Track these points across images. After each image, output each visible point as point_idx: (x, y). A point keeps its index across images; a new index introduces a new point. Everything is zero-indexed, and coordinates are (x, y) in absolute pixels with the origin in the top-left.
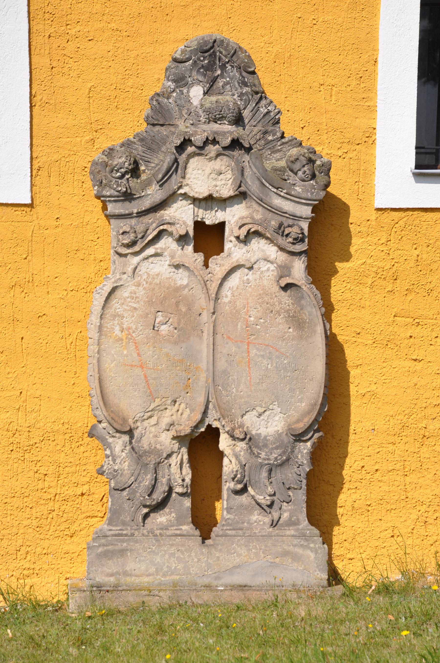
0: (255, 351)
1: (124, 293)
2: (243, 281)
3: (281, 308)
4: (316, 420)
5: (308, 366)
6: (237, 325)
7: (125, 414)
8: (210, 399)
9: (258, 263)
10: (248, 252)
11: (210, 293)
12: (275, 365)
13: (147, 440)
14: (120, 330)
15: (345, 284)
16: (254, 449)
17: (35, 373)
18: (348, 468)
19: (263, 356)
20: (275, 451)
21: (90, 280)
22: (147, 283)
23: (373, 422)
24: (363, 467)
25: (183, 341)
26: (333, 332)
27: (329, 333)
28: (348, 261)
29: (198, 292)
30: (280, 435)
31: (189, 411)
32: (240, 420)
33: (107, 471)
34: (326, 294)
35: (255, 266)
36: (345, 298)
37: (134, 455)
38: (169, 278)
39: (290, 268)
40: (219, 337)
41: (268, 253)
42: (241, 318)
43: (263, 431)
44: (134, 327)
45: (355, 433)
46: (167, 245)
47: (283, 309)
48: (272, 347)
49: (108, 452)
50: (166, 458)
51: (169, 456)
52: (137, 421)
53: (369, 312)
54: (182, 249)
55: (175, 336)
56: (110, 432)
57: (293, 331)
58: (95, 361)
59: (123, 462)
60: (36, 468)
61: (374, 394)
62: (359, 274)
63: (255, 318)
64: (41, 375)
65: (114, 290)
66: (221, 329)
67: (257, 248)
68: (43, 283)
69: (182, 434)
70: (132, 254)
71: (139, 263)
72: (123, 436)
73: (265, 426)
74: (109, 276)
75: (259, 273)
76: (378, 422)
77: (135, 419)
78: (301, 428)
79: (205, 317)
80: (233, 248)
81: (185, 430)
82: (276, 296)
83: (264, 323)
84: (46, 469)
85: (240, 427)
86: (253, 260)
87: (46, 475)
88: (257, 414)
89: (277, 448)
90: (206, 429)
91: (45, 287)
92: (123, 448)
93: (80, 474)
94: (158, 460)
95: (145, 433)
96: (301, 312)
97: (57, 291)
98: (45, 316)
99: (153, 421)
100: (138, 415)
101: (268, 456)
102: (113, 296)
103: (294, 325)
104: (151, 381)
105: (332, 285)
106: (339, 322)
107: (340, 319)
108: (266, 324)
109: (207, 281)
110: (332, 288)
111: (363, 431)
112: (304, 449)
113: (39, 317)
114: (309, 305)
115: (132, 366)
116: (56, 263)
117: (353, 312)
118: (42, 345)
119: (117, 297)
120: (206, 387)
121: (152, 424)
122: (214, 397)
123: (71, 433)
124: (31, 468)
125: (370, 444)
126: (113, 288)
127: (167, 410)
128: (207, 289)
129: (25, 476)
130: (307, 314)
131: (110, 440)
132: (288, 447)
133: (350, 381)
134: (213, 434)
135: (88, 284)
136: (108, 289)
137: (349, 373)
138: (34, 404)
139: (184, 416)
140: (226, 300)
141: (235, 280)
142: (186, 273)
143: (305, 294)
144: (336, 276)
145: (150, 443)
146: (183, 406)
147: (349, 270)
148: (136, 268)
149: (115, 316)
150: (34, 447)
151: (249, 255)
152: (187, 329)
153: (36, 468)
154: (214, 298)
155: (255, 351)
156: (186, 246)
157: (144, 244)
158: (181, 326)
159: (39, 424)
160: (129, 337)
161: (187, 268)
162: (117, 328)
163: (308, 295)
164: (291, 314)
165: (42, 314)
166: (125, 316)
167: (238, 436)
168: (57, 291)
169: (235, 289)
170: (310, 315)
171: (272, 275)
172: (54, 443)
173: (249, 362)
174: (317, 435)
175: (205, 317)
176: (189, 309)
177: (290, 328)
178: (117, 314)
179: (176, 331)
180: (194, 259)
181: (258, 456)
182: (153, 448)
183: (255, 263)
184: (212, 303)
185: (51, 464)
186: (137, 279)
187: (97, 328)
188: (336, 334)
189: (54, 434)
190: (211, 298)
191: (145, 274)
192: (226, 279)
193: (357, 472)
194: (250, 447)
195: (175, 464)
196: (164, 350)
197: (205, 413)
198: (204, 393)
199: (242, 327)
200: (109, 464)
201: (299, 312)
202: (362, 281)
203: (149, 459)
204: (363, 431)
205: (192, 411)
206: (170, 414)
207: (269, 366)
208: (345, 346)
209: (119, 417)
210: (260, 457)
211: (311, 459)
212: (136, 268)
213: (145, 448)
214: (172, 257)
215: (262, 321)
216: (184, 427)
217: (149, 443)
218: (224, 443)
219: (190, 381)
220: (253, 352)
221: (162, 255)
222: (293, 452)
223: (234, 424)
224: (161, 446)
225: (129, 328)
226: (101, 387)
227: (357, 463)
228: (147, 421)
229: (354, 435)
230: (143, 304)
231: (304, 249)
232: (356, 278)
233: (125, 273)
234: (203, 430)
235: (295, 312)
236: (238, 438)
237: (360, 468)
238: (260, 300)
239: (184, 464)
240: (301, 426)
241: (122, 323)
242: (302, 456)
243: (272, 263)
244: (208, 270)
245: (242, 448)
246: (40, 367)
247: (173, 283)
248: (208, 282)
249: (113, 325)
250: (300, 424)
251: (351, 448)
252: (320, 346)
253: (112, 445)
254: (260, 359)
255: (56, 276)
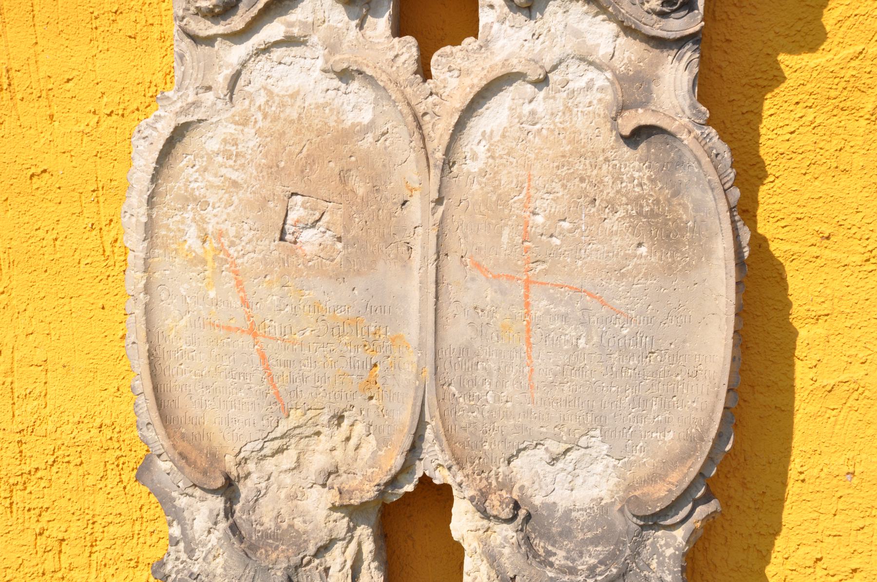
0: (545, 302)
1: (205, 142)
2: (520, 117)
3: (618, 192)
4: (701, 474)
5: (684, 342)
6: (500, 234)
7: (215, 444)
8: (427, 418)
9: (562, 67)
10: (536, 36)
11: (430, 146)
12: (596, 339)
13: (270, 507)
14: (199, 237)
15: (799, 111)
16: (537, 541)
17: (30, 308)
18: (780, 560)
19: (564, 317)
20: (590, 548)
21: (153, 89)
22: (265, 117)
23: (850, 455)
24: (819, 559)
25: (358, 273)
26: (760, 231)
27: (746, 254)
28: (813, 49)
29: (401, 142)
30: (605, 510)
31: (374, 443)
32: (503, 469)
33: (173, 576)
34: (748, 137)
35: (553, 77)
36: (796, 146)
37: (237, 545)
38: (325, 106)
39: (649, 82)
40: (451, 263)
41: (591, 40)
42: (510, 216)
43: (562, 499)
44: (232, 231)
45: (803, 481)
46: (320, 15)
47: (625, 195)
48: (590, 295)
49: (176, 531)
50: (315, 556)
51: (323, 550)
52: (246, 460)
53: (861, 183)
54: (361, 26)
55: (338, 259)
56: (180, 484)
57: (650, 251)
58: (139, 311)
59: (210, 557)
60: (40, 525)
61: (857, 389)
62: (843, 84)
63: (548, 218)
64: (47, 313)
65: (179, 133)
66: (455, 243)
67: (561, 27)
68: (36, 94)
69: (356, 501)
70: (226, 36)
71: (246, 61)
72: (209, 496)
73: (567, 485)
74: (169, 94)
75: (565, 95)
76: (864, 456)
77: (242, 455)
78: (659, 499)
79: (416, 210)
80: (496, 26)
81: (362, 491)
82: (607, 160)
83: (571, 231)
84: (63, 529)
85: (501, 486)
86: (548, 61)
87: (63, 540)
88: (547, 457)
89: (595, 541)
90: (417, 487)
91: (43, 102)
92: (210, 525)
93: (142, 540)
94: (295, 560)
95: (267, 488)
96: (675, 201)
97: (74, 115)
98: (46, 175)
99: (287, 460)
100: (249, 447)
101: (573, 561)
102: (179, 148)
103: (652, 238)
104: (276, 370)
105: (766, 114)
106: (777, 206)
107: (779, 199)
108: (577, 234)
109: (425, 114)
110: (764, 122)
111: (823, 475)
112: (667, 545)
113: (32, 176)
114: (698, 183)
115: (229, 328)
116: (66, 43)
117: (817, 183)
118: (45, 243)
119: (190, 149)
120: (417, 388)
121: (285, 466)
122: (437, 414)
123: (120, 448)
124: (27, 525)
125: (841, 507)
126: (176, 128)
127: (322, 437)
128: (423, 138)
129: (15, 542)
130: (690, 206)
131: (182, 502)
132: (624, 543)
133: (796, 353)
134: (436, 497)
135: (148, 100)
136: (165, 130)
137: (795, 333)
138: (31, 381)
139: (362, 451)
140: (473, 167)
141: (496, 115)
142: (369, 94)
143: (688, 154)
144: (776, 91)
145: (279, 514)
146: (360, 428)
147: (815, 74)
148: (237, 76)
149: (189, 199)
150: (33, 478)
151: (538, 45)
152: (370, 239)
153: (40, 525)
154: (440, 163)
155: (545, 302)
156: (370, 19)
157: (255, 11)
158: (353, 233)
159: (44, 426)
160: (221, 255)
161: (370, 80)
162: (192, 231)
163: (695, 157)
164: (647, 209)
165: (39, 171)
166: (211, 201)
167: (495, 513)
168: (74, 115)
169: (497, 138)
170: (697, 209)
171: (600, 100)
172: (81, 471)
173: (529, 331)
174: (702, 511)
175: (416, 210)
176: (376, 189)
177: (640, 245)
178: (191, 194)
179: (339, 246)
180: (391, 55)
181: (546, 563)
182: (285, 525)
183: (555, 68)
184: (435, 174)
185: (75, 518)
186: (241, 105)
187: (142, 229)
188: (768, 236)
189: (79, 449)
190: (432, 162)
191: (262, 92)
192: (475, 110)
193: (803, 571)
194: (527, 538)
195: (338, 567)
196: (310, 295)
197: (414, 450)
198: (411, 402)
199: (511, 239)
200: (177, 559)
201: (669, 201)
202: (848, 104)
203: (274, 556)
204: (823, 475)
205: (383, 442)
206: (329, 446)
207: (582, 341)
208: (790, 269)
209: (201, 451)
210: (551, 565)
211: (684, 570)
212: (237, 76)
213: (267, 525)
214: (332, 48)
215: (566, 225)
216: (361, 483)
217: (275, 513)
218: (463, 522)
219: (378, 368)
220: (540, 305)
221: (304, 43)
222: (636, 554)
223: (487, 479)
224: (305, 522)
225: (221, 234)
226: (154, 375)
227: (803, 550)
228: (272, 461)
229: (799, 484)
230: (255, 173)
231: (691, 31)
232: (833, 94)
233: (209, 88)
234: (409, 488)
235: (657, 202)
236: (495, 517)
237: (811, 563)
238: (563, 172)
239: (366, 564)
240: (660, 494)
241: (203, 220)
242: (661, 564)
243: (600, 67)
244: (430, 84)
245: (505, 538)
246: (42, 295)
247: (334, 118)
248: (427, 118)
249: (183, 222)
250: (658, 487)
251: (790, 515)
252: (722, 290)
253: (186, 514)
254: (558, 324)
255: (67, 77)
